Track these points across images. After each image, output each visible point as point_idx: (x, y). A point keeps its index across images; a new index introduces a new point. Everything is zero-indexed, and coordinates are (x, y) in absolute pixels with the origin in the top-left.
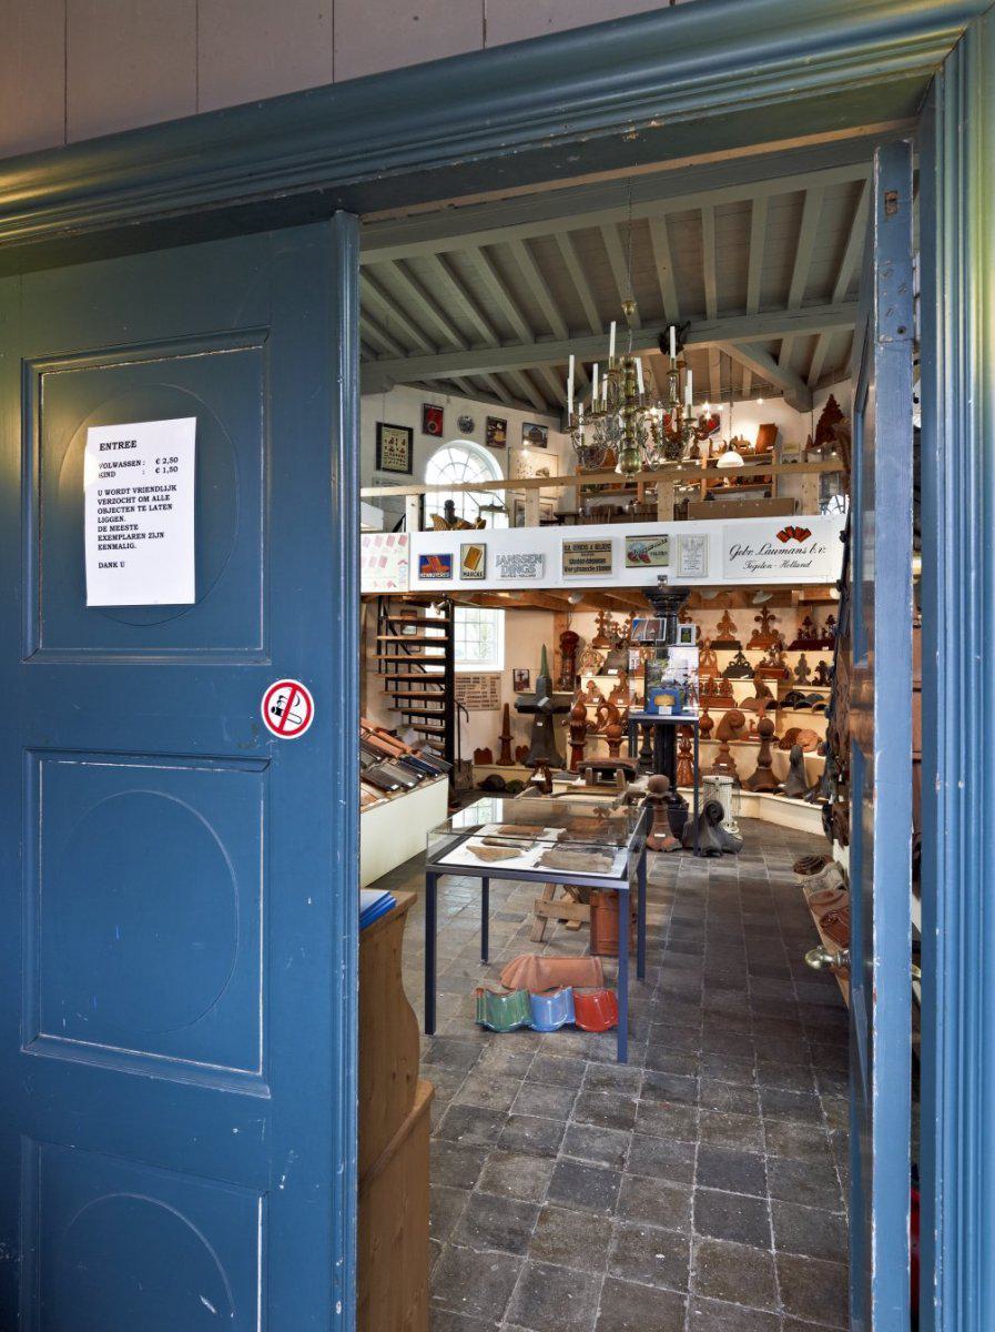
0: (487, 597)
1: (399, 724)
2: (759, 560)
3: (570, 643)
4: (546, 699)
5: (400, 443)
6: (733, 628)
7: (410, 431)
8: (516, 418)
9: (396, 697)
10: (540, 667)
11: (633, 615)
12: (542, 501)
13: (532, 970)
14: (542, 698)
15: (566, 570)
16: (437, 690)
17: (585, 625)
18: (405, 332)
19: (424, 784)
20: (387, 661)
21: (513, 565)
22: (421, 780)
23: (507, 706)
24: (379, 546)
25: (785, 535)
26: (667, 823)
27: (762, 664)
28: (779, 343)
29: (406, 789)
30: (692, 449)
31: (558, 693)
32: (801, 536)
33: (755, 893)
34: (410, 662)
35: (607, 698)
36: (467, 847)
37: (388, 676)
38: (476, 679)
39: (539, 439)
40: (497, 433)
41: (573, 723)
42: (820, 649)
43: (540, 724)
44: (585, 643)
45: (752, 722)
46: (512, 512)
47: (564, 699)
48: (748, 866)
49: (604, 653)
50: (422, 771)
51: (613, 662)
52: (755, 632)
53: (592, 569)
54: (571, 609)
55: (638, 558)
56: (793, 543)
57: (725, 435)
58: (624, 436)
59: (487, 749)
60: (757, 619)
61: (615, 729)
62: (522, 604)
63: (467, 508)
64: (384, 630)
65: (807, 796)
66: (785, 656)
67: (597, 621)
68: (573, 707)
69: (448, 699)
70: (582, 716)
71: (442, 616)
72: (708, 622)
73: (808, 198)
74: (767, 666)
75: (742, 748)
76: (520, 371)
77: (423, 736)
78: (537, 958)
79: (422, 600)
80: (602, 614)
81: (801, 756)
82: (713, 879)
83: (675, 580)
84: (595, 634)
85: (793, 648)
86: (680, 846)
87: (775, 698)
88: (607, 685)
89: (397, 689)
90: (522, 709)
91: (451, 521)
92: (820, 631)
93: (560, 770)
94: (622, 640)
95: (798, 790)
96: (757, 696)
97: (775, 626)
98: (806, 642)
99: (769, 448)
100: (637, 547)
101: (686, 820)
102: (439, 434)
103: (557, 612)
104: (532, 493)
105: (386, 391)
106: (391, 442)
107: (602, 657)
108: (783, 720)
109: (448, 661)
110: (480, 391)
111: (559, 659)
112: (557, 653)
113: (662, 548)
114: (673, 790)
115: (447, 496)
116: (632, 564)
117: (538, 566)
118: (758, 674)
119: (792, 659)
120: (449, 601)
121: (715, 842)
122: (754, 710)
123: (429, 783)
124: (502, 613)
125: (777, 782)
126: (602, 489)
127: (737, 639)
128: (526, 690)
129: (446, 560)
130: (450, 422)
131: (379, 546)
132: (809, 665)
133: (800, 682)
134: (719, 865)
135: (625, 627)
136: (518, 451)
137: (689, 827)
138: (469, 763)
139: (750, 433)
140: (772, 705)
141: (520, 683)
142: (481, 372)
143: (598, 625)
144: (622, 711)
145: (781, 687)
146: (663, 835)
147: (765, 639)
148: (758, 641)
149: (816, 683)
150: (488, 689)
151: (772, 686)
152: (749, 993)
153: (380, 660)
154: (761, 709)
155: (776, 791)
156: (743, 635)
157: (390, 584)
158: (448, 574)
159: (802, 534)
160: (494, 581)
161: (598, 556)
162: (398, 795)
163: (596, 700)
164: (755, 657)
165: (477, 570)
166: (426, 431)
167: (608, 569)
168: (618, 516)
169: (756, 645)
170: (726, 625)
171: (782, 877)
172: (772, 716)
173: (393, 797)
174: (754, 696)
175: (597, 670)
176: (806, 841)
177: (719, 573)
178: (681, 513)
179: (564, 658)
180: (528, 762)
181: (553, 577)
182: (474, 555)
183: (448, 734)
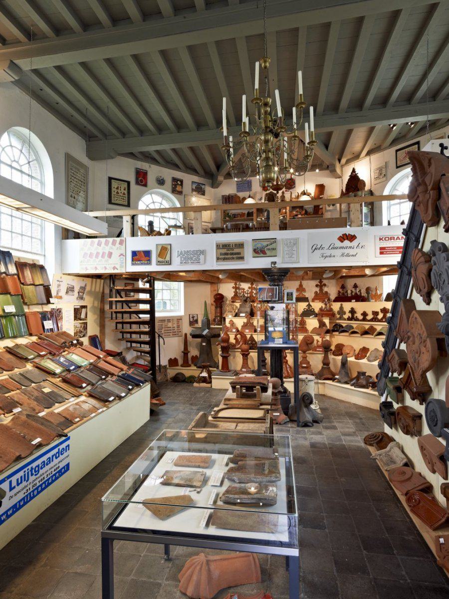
0: (174, 276)
1: (125, 347)
2: (328, 253)
3: (219, 300)
4: (207, 330)
5: (122, 189)
6: (304, 290)
7: (129, 183)
8: (188, 179)
9: (123, 333)
10: (203, 313)
11: (252, 284)
12: (203, 224)
13: (204, 577)
14: (205, 330)
15: (218, 259)
16: (146, 328)
17: (227, 290)
18: (127, 127)
19: (133, 392)
20: (116, 313)
21: (187, 256)
22: (130, 390)
23: (186, 335)
24: (107, 246)
25: (343, 238)
26: (280, 406)
27: (321, 309)
28: (329, 135)
29: (120, 398)
30: (281, 197)
31: (213, 326)
32: (351, 239)
33: (339, 453)
34: (130, 313)
35: (240, 329)
36: (145, 503)
37: (117, 321)
38: (169, 320)
39: (200, 190)
40: (178, 186)
41: (222, 344)
42: (351, 301)
43: (204, 344)
44: (227, 299)
45: (318, 341)
46: (187, 229)
47: (217, 330)
48: (327, 433)
49: (238, 305)
50: (130, 383)
51: (243, 309)
52: (316, 293)
53: (233, 258)
54: (219, 281)
55: (259, 252)
56: (347, 243)
57: (299, 189)
58: (264, 155)
59: (175, 358)
60: (317, 286)
61: (245, 347)
62: (193, 279)
63: (160, 225)
64: (114, 296)
65: (352, 383)
66: (332, 305)
67: (233, 288)
68: (222, 335)
69: (152, 333)
70: (227, 340)
71: (147, 286)
72: (290, 287)
73: (365, 21)
74: (323, 311)
75: (313, 355)
76: (188, 147)
77: (139, 354)
78: (208, 562)
79: (135, 277)
80: (236, 284)
81: (347, 360)
82: (313, 445)
83: (281, 265)
84: (233, 295)
85: (336, 300)
86: (288, 420)
87: (328, 328)
88: (240, 322)
89: (123, 328)
90: (194, 336)
91: (151, 231)
92: (349, 292)
93: (215, 369)
94: (247, 297)
95: (346, 379)
96: (320, 327)
97: (325, 289)
98: (342, 298)
99: (321, 196)
100: (259, 245)
101: (290, 403)
102: (145, 185)
103: (212, 283)
104: (198, 214)
105: (113, 158)
106: (117, 188)
107: (237, 307)
108: (333, 339)
109: (152, 312)
110: (171, 164)
111: (213, 308)
112: (212, 305)
113: (273, 246)
114: (282, 385)
115: (150, 218)
116: (257, 255)
117: (202, 257)
118: (320, 315)
119: (336, 306)
120: (151, 278)
121: (309, 418)
122: (318, 334)
123: (137, 390)
124: (182, 284)
125: (334, 375)
126: (235, 217)
127: (307, 296)
128: (196, 326)
129: (147, 254)
130: (151, 179)
131: (107, 246)
132: (345, 310)
133: (341, 318)
134: (313, 433)
135: (248, 291)
136: (189, 197)
137: (292, 407)
138: (165, 366)
139: (311, 189)
140: (328, 332)
141: (193, 322)
142: (166, 148)
143: (234, 290)
144: (248, 336)
145: (332, 321)
146: (278, 414)
147: (321, 296)
148: (318, 297)
149: (349, 319)
150: (175, 326)
151: (327, 321)
152: (371, 577)
153: (112, 312)
154: (323, 334)
155: (333, 379)
156: (309, 294)
157: (87, 269)
158: (149, 262)
159: (352, 238)
160: (176, 266)
161: (236, 251)
162: (115, 402)
163: (234, 330)
164: (317, 306)
165: (166, 260)
166: (137, 183)
167: (242, 258)
168: (247, 229)
169: (317, 299)
170: (301, 289)
171: (352, 441)
172: (328, 338)
173: (110, 406)
174: (318, 327)
175: (234, 314)
176: (354, 410)
177: (306, 261)
178: (283, 226)
179: (216, 307)
180: (198, 365)
181: (211, 263)
182: (164, 251)
183: (152, 353)
